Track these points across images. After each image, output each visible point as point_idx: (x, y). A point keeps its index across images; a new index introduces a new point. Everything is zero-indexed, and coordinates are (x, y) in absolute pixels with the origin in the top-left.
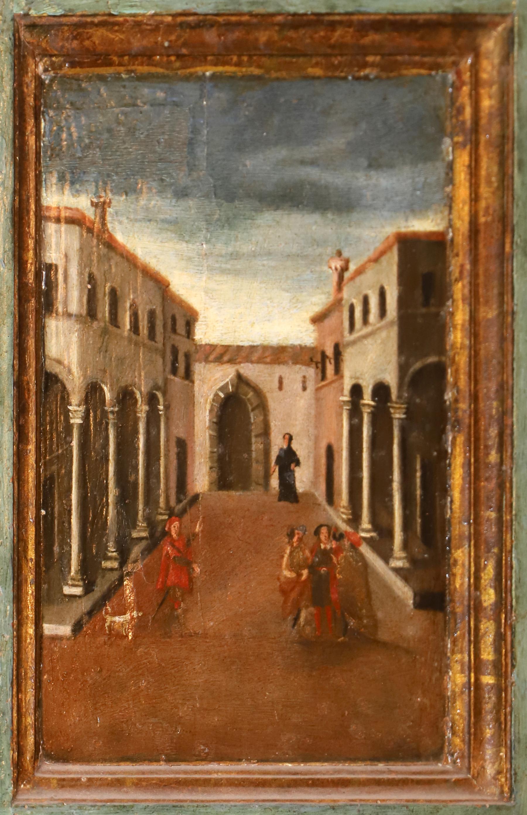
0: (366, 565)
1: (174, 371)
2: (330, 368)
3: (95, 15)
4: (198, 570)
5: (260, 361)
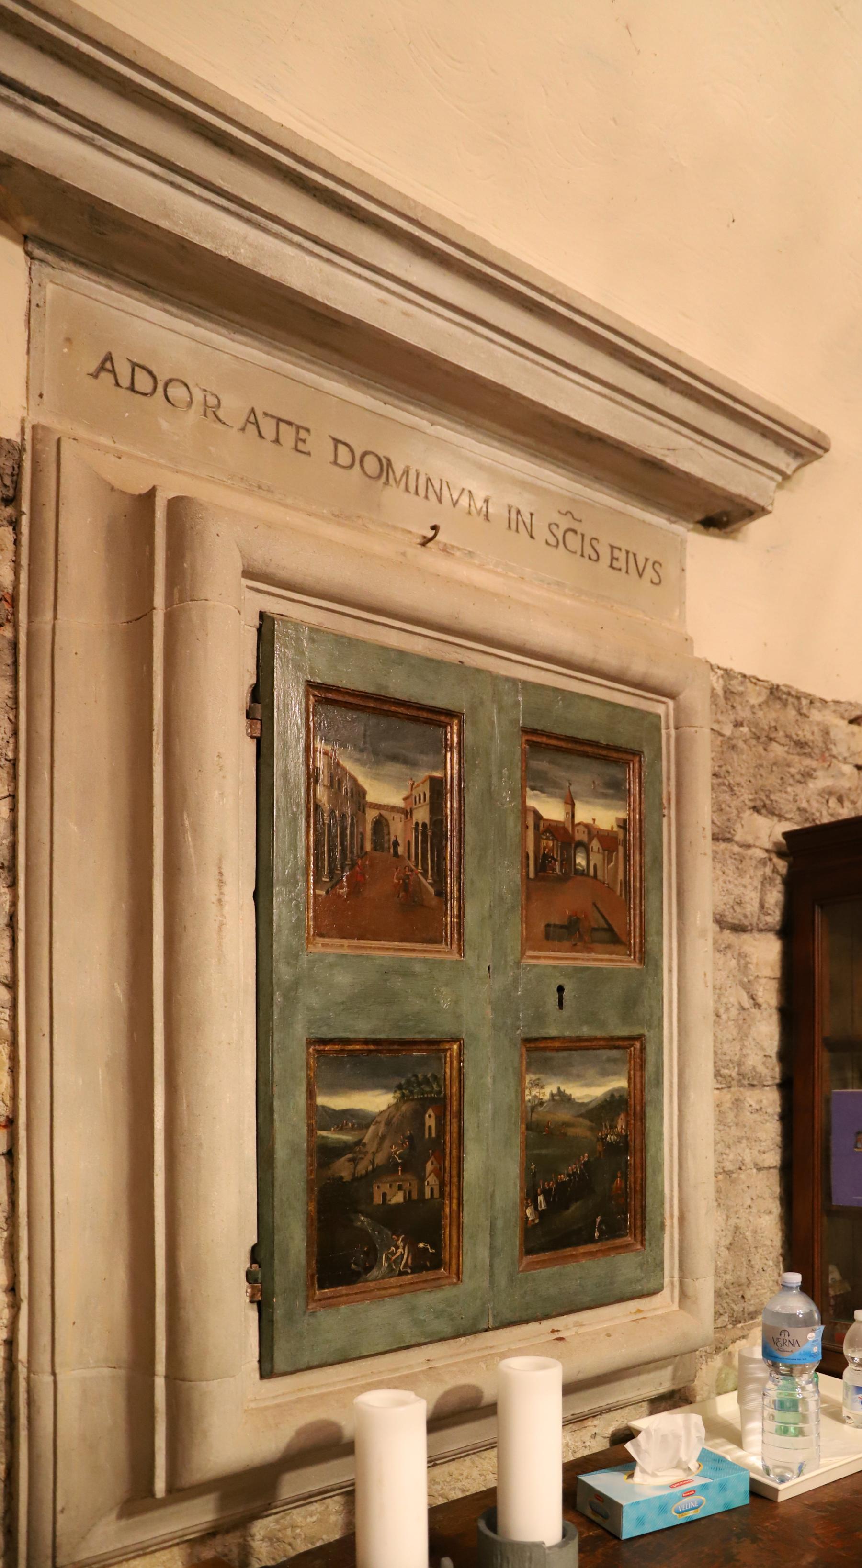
0: (420, 880)
1: (359, 810)
2: (409, 816)
3: (334, 686)
4: (367, 877)
5: (387, 810)
